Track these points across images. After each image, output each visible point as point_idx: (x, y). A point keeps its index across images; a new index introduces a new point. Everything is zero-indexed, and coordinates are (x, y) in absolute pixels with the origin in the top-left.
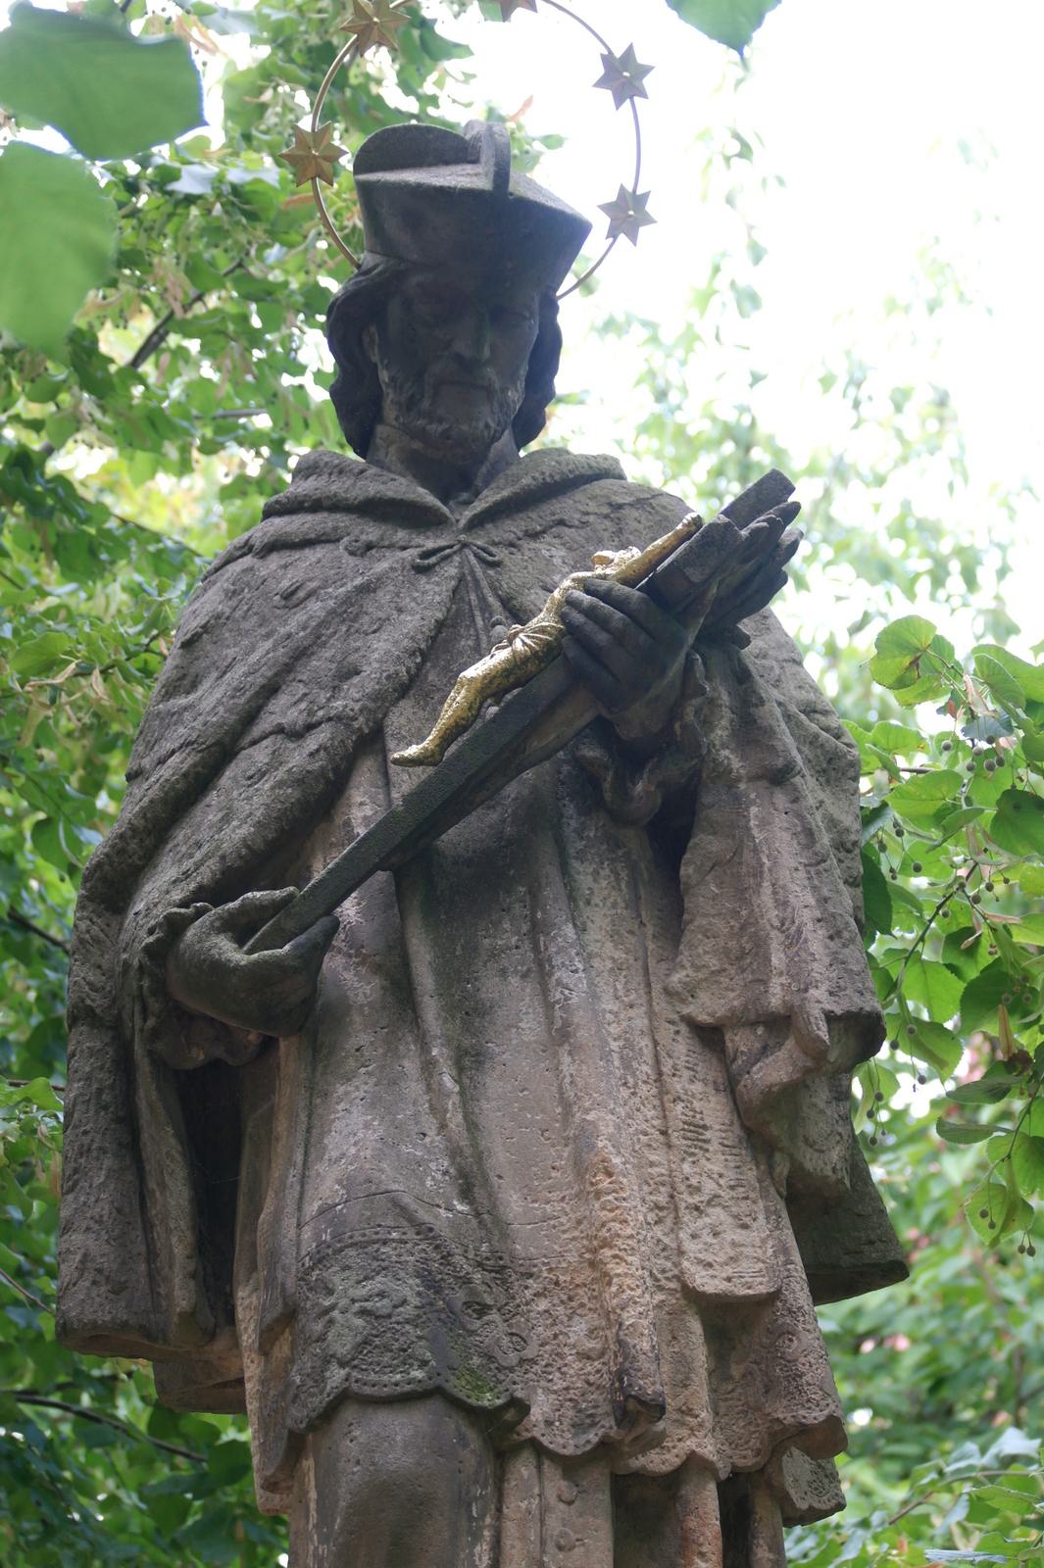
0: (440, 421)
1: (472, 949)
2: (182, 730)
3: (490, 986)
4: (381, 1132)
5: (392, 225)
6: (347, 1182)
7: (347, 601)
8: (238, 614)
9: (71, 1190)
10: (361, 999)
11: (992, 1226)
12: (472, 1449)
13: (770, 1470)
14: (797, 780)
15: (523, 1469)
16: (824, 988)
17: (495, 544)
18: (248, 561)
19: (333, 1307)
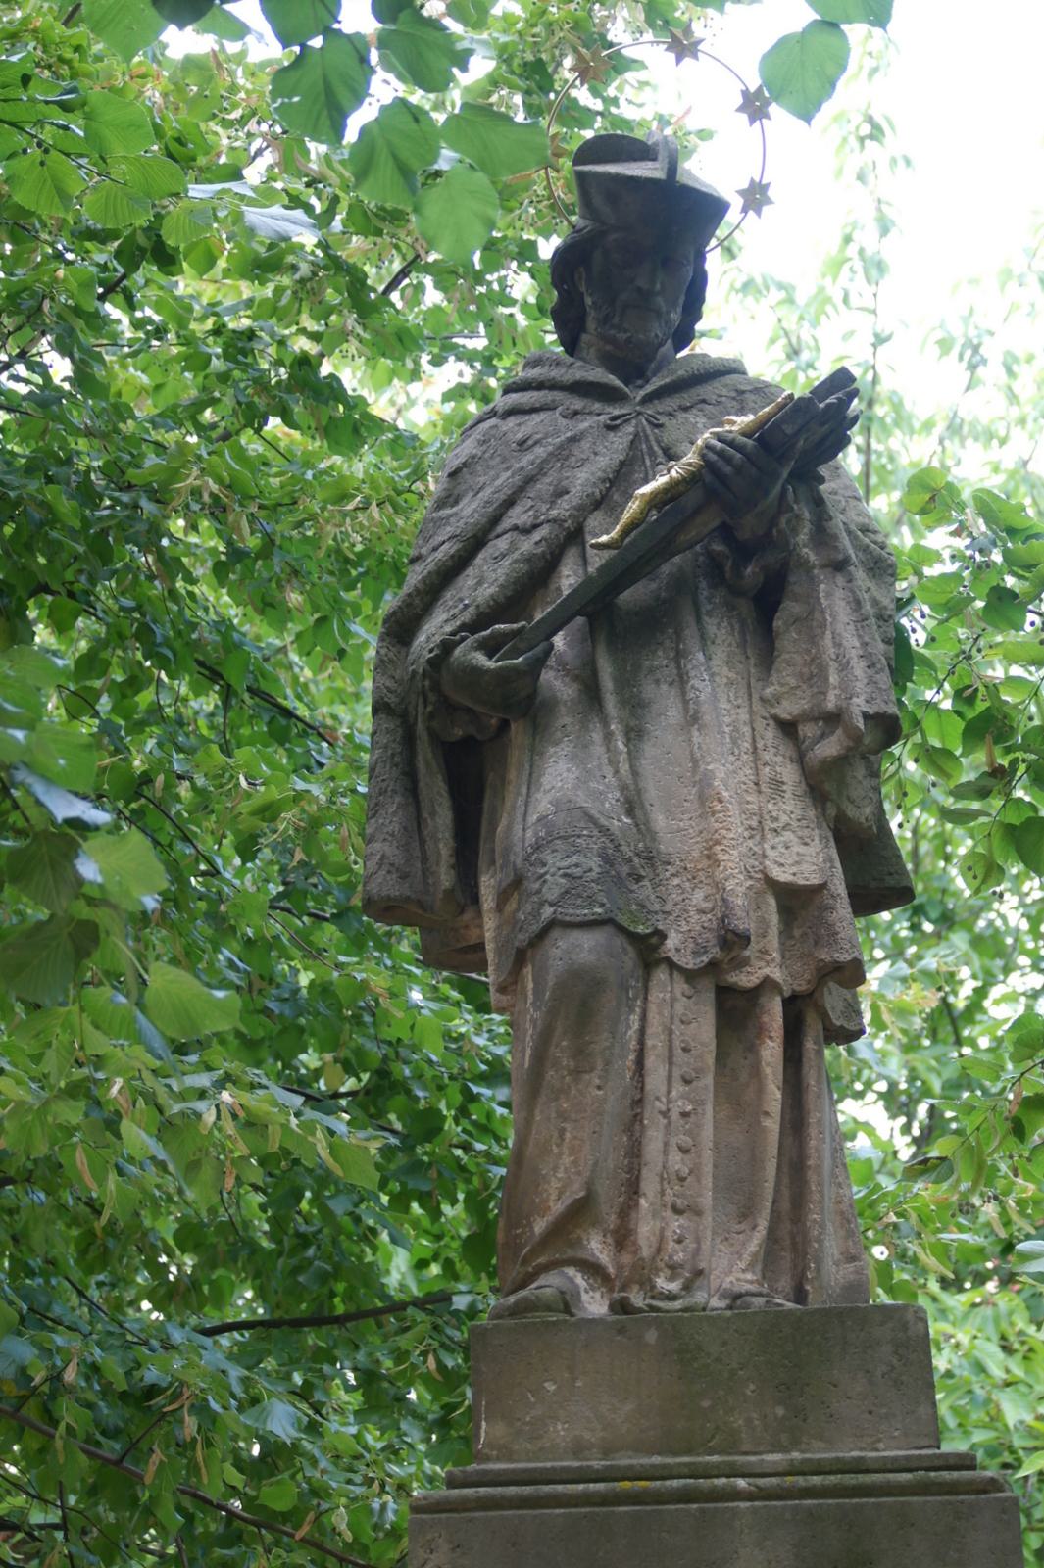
0: (626, 331)
1: (637, 667)
2: (449, 529)
3: (648, 690)
4: (577, 774)
5: (598, 201)
6: (556, 803)
7: (561, 447)
8: (487, 455)
9: (374, 816)
10: (565, 697)
11: (975, 877)
12: (630, 958)
13: (816, 995)
14: (852, 568)
15: (661, 975)
16: (862, 697)
17: (659, 413)
18: (493, 421)
19: (546, 873)
